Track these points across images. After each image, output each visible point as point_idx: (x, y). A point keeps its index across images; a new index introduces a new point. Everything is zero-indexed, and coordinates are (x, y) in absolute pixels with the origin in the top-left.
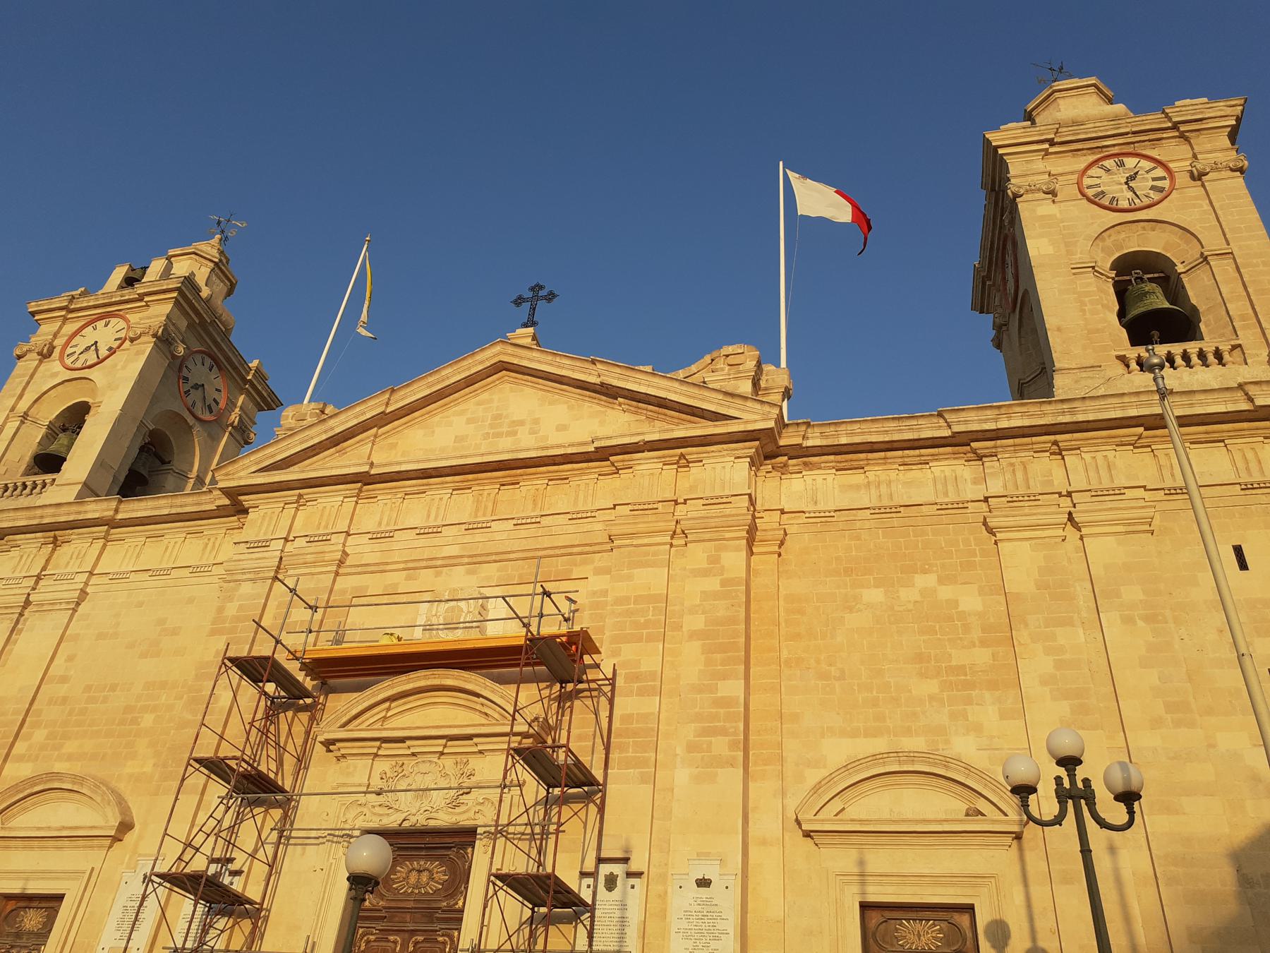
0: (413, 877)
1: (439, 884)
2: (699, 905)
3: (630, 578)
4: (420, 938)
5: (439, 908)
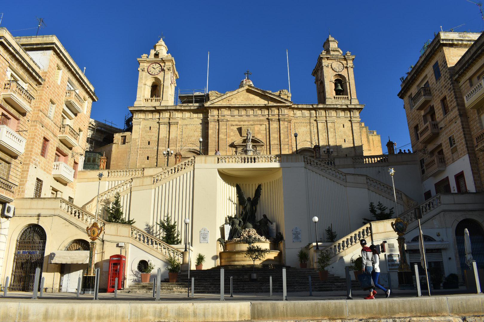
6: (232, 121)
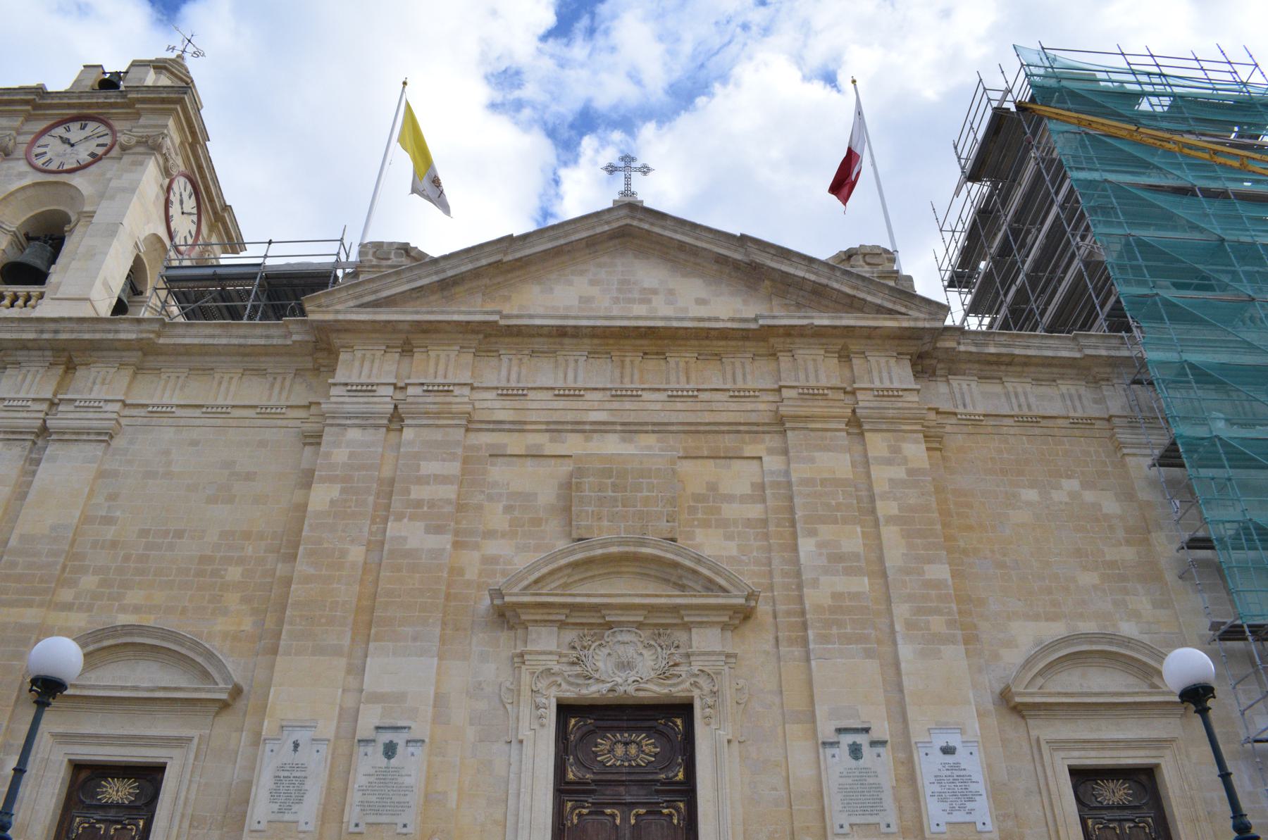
0: (620, 750)
1: (651, 756)
2: (947, 770)
3: (812, 460)
4: (642, 811)
5: (658, 781)
6: (498, 426)
